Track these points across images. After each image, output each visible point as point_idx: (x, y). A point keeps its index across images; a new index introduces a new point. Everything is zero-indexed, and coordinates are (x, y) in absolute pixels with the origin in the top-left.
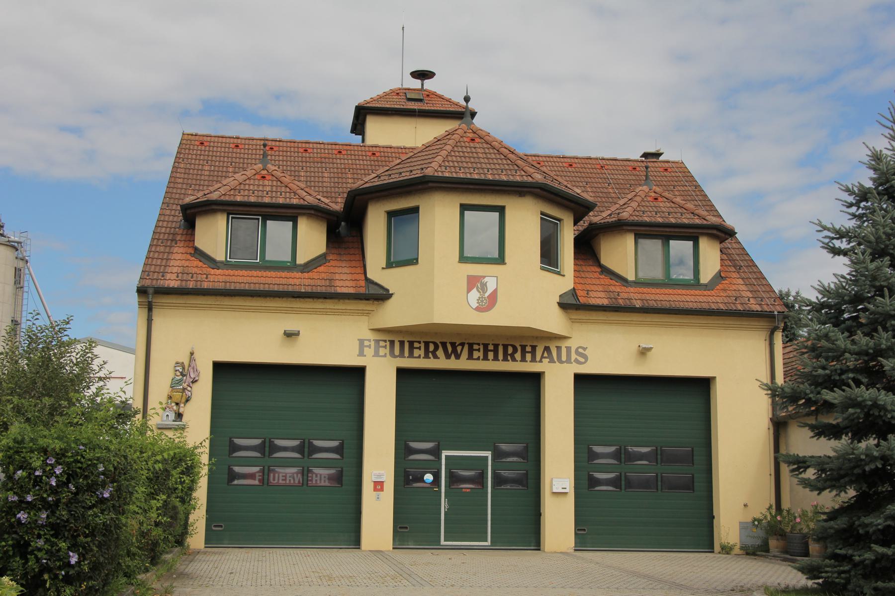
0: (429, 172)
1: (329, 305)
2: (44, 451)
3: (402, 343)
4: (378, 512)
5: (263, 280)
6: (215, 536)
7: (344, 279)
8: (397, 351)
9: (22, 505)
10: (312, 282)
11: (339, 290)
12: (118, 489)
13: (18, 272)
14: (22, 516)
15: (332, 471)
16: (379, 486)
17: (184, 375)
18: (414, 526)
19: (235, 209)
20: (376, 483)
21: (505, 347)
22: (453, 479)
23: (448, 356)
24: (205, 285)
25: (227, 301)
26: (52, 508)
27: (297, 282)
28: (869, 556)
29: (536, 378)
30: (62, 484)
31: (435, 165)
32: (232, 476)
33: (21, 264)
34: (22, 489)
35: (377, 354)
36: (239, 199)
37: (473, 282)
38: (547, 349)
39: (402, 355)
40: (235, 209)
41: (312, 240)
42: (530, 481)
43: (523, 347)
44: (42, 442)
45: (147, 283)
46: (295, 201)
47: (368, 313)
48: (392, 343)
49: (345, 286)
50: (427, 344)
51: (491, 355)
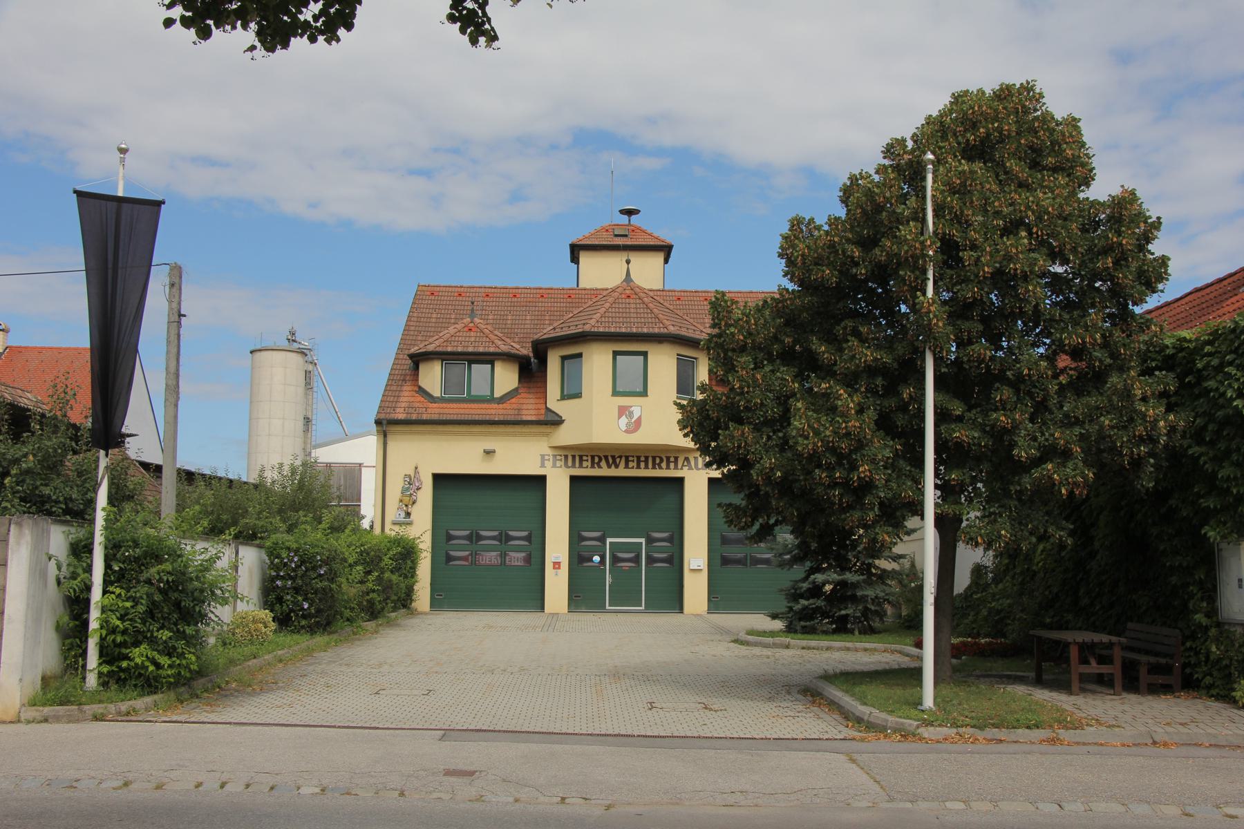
0: (587, 328)
1: (518, 429)
2: (289, 549)
3: (574, 457)
4: (557, 585)
5: (467, 411)
6: (438, 602)
7: (529, 408)
8: (570, 464)
9: (278, 577)
10: (505, 412)
11: (525, 418)
12: (331, 570)
13: (308, 374)
14: (279, 583)
15: (523, 554)
16: (557, 565)
17: (411, 484)
18: (583, 595)
19: (445, 357)
20: (555, 563)
21: (654, 458)
22: (615, 560)
23: (609, 466)
24: (425, 417)
25: (440, 428)
26: (293, 579)
27: (493, 412)
28: (799, 606)
29: (680, 481)
30: (298, 567)
31: (593, 322)
32: (449, 559)
33: (310, 367)
34: (277, 569)
35: (554, 466)
36: (449, 349)
37: (623, 411)
38: (687, 459)
39: (574, 466)
40: (445, 357)
41: (506, 378)
42: (676, 560)
43: (668, 458)
44: (287, 544)
45: (382, 416)
46: (492, 350)
47: (547, 435)
48: (566, 457)
49: (529, 416)
50: (593, 457)
51: (642, 465)
